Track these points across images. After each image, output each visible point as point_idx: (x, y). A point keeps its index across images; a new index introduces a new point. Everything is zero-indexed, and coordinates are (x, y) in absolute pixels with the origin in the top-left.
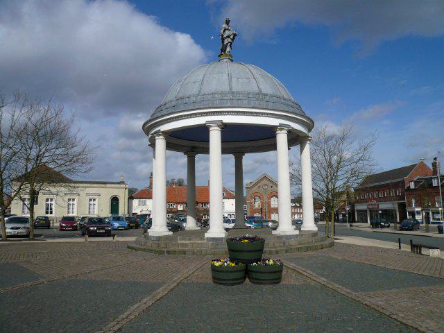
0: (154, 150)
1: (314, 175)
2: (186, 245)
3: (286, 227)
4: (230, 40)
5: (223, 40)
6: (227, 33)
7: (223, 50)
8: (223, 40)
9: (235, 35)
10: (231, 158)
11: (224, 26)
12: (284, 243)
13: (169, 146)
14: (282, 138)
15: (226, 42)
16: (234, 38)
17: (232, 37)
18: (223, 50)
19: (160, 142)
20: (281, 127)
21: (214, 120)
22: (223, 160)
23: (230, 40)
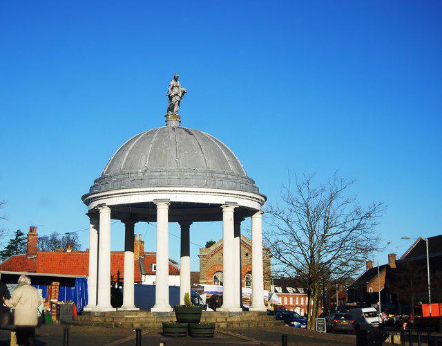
0: (97, 227)
1: (266, 276)
2: (133, 318)
3: (231, 304)
4: (178, 99)
5: (171, 98)
6: (176, 90)
7: (171, 109)
8: (171, 98)
9: (184, 93)
10: (177, 226)
11: (173, 83)
12: (226, 319)
13: (113, 216)
14: (228, 214)
15: (174, 99)
16: (183, 94)
17: (180, 95)
18: (171, 109)
19: (105, 214)
20: (227, 204)
21: (163, 196)
22: (169, 227)
23: (178, 99)
